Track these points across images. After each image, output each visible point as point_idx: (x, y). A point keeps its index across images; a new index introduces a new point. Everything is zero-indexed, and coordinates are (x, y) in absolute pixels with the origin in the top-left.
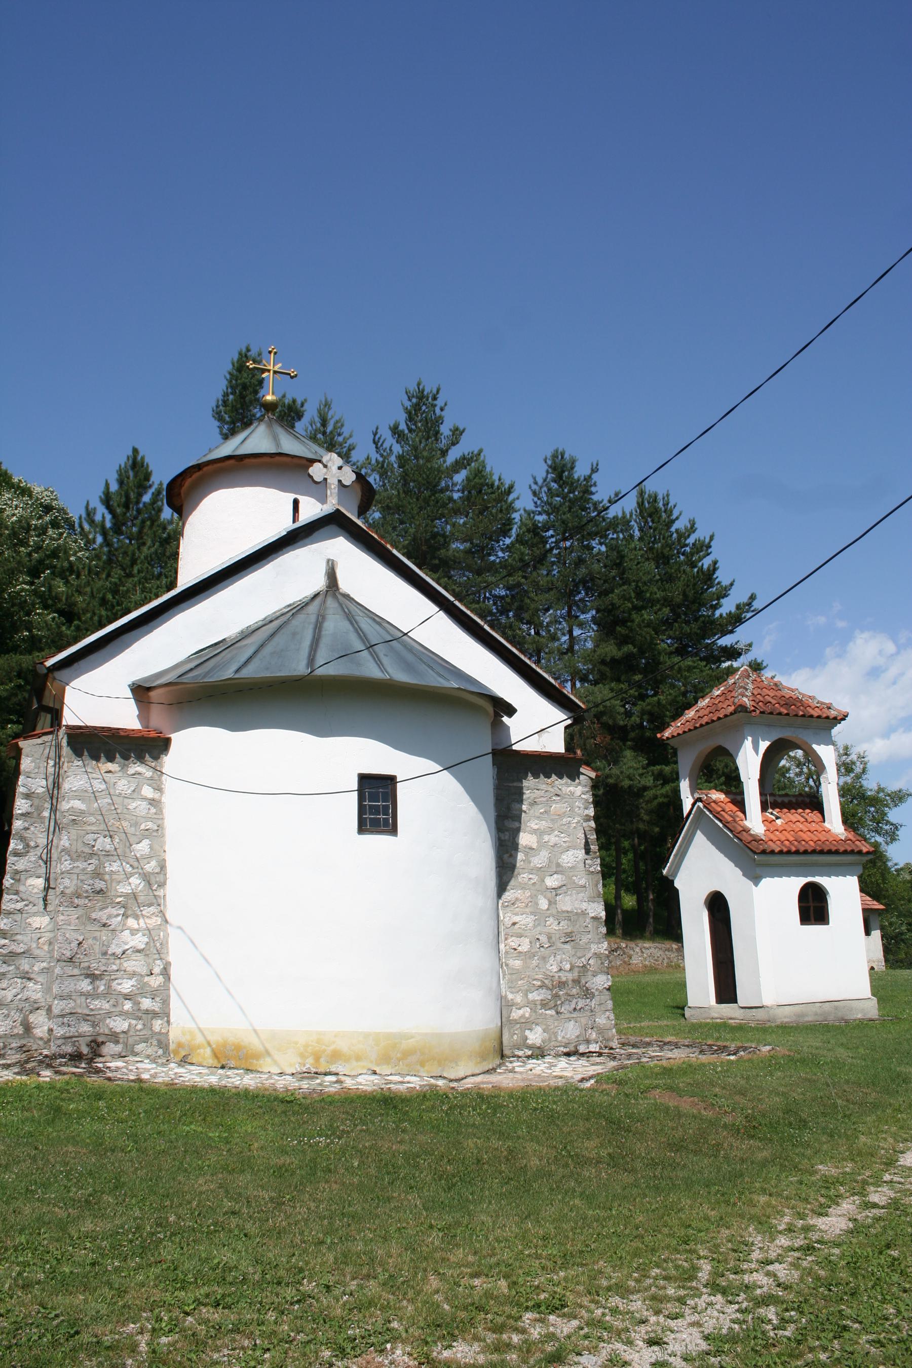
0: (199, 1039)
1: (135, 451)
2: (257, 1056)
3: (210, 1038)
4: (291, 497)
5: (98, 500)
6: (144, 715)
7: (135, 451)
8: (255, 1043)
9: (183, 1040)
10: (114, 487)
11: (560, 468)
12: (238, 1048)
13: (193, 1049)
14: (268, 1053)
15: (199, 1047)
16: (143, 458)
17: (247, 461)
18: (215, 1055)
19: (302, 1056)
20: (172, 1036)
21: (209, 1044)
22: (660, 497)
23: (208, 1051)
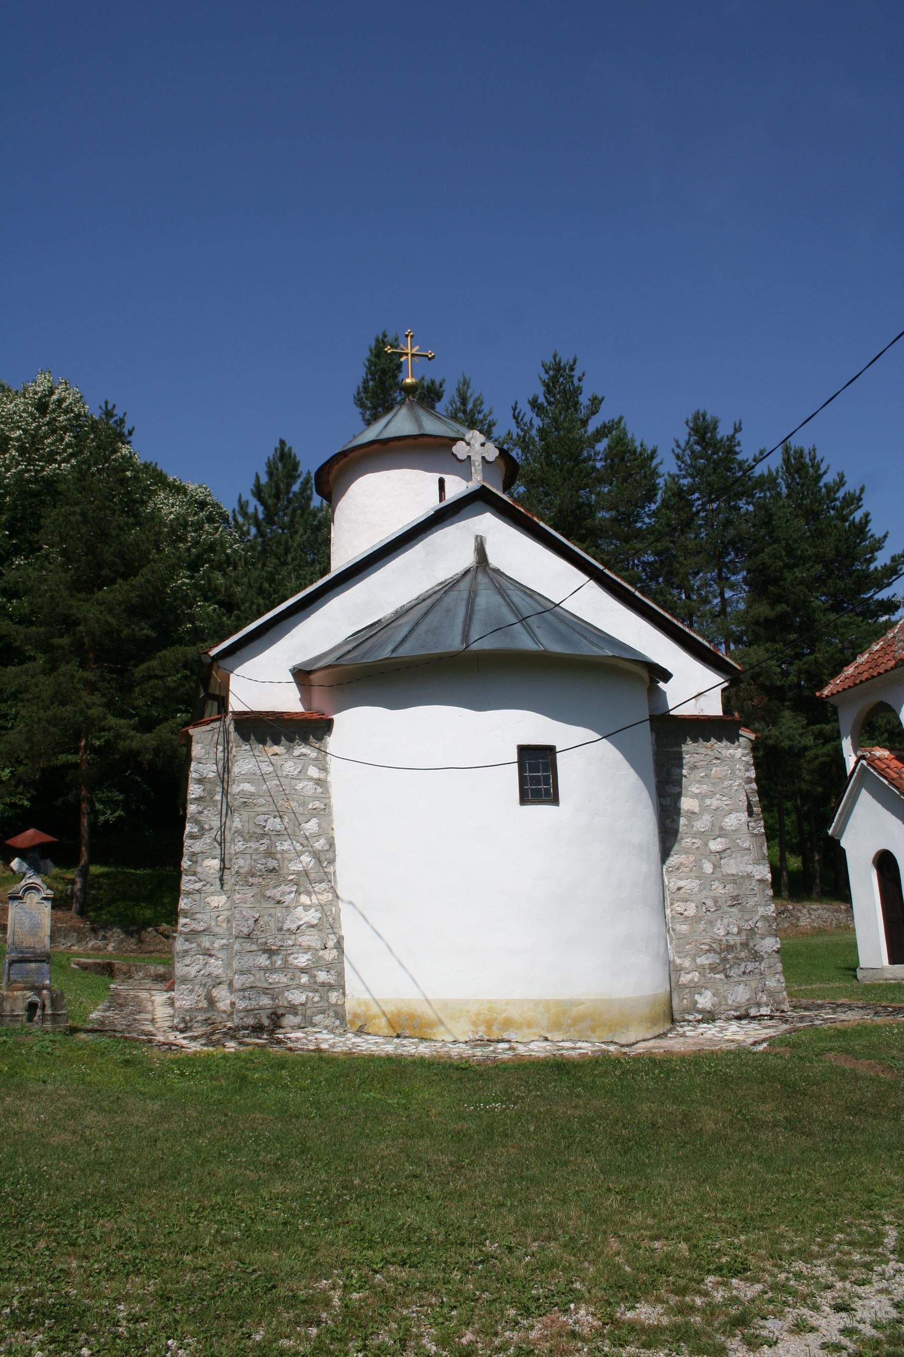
0: (375, 1010)
1: (282, 443)
2: (431, 1025)
3: (384, 1008)
5: (250, 492)
6: (306, 699)
8: (428, 1013)
10: (264, 479)
12: (412, 1017)
13: (369, 1019)
14: (441, 1022)
15: (374, 1017)
16: (290, 449)
17: (391, 444)
18: (391, 1024)
19: (474, 1024)
20: (348, 1007)
21: (384, 1014)
23: (383, 1021)
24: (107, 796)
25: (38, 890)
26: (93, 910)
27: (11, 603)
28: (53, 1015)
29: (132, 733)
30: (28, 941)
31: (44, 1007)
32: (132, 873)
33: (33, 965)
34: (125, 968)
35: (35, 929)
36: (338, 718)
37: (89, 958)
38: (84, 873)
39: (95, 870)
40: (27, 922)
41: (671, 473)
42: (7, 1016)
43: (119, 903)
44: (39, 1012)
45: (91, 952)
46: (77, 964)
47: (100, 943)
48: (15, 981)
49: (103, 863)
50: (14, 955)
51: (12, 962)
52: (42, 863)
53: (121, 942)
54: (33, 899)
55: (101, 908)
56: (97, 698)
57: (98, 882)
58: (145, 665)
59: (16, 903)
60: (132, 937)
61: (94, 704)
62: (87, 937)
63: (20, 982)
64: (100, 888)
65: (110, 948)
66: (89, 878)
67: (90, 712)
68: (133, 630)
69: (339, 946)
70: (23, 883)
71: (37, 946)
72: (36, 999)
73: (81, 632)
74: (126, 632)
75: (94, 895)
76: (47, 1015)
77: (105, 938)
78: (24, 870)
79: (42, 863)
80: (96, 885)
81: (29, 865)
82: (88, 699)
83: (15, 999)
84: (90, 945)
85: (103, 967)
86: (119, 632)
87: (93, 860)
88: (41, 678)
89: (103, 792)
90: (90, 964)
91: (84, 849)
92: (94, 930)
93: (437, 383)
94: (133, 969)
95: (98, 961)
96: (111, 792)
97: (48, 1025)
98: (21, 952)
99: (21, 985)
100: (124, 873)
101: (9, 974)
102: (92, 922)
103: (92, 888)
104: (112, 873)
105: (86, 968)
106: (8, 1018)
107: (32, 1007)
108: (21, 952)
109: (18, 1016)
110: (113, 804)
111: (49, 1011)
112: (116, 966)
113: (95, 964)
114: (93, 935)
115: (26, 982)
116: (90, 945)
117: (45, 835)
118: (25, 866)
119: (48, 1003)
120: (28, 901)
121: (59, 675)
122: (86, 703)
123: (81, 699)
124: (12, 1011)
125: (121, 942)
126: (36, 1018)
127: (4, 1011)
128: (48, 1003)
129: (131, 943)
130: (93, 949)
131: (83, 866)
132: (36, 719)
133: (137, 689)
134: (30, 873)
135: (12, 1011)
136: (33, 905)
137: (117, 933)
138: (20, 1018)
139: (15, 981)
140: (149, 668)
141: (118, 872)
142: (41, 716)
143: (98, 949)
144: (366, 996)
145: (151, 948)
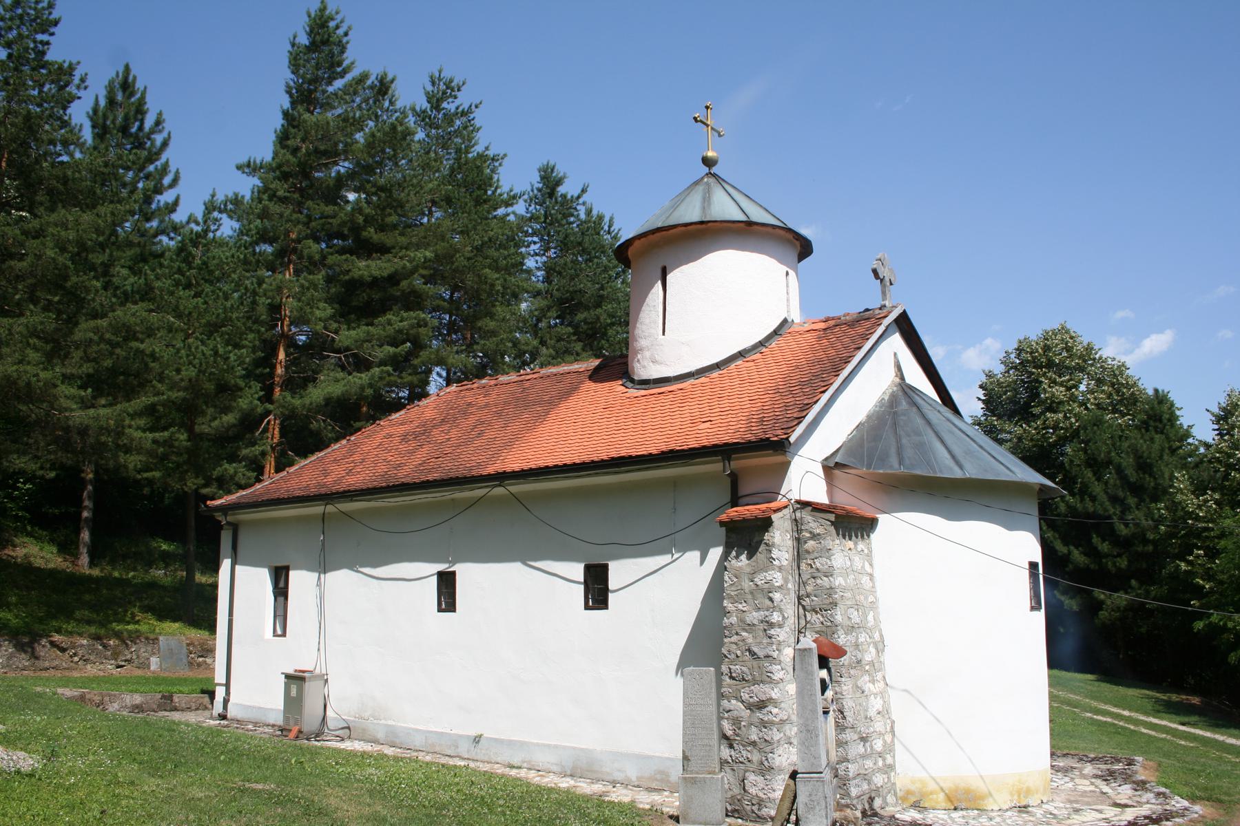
0: (932, 786)
1: (127, 69)
2: (982, 798)
3: (942, 784)
4: (785, 268)
5: (84, 115)
6: (830, 493)
7: (127, 69)
8: (977, 785)
9: (913, 788)
10: (102, 103)
11: (550, 181)
12: (968, 792)
13: (924, 795)
14: (990, 794)
15: (931, 793)
16: (135, 78)
17: (756, 227)
18: (949, 799)
19: (1012, 794)
20: (898, 786)
21: (942, 789)
22: (607, 219)
23: (941, 796)
36: (883, 519)
41: (77, 102)
69: (893, 731)
93: (390, 77)
94: (106, 699)
117: (1116, 688)
129: (23, 660)
144: (923, 775)
145: (47, 664)
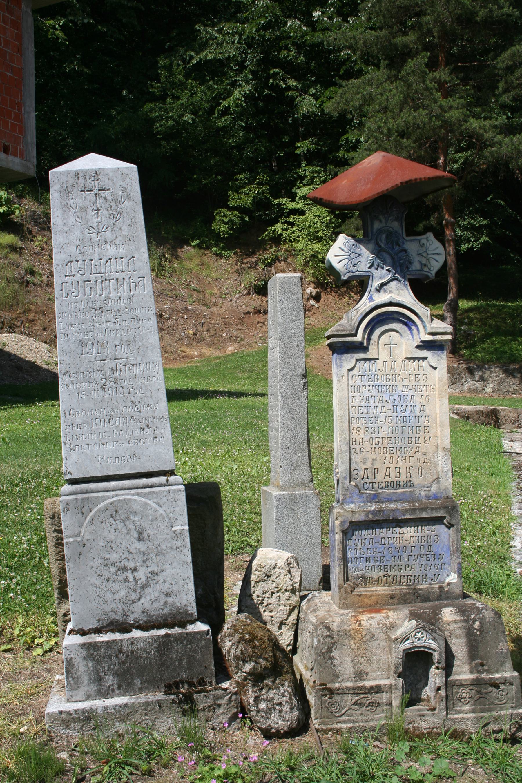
24: (469, 223)
25: (408, 323)
26: (466, 348)
27: (348, 22)
28: (477, 683)
29: (499, 137)
30: (391, 467)
31: (448, 668)
32: (504, 307)
33: (409, 533)
34: (513, 416)
35: (408, 431)
37: (469, 404)
38: (454, 308)
39: (464, 304)
40: (385, 416)
42: (343, 692)
43: (494, 339)
44: (435, 677)
45: (468, 395)
46: (457, 414)
47: (478, 385)
48: (365, 580)
49: (470, 297)
50: (357, 509)
51: (352, 528)
52: (412, 247)
53: (501, 382)
54: (396, 346)
55: (474, 345)
56: (455, 101)
57: (468, 318)
58: (509, 52)
59: (349, 360)
60: (514, 377)
61: (451, 107)
62: (462, 378)
63: (377, 582)
64: (470, 323)
65: (489, 389)
66: (459, 312)
67: (447, 115)
68: (491, 11)
70: (365, 304)
71: (416, 480)
72: (425, 641)
73: (427, 23)
74: (482, 13)
75: (465, 332)
76: (460, 684)
77: (482, 379)
78: (363, 267)
79: (412, 247)
80: (466, 321)
81: (378, 252)
82: (443, 102)
83: (366, 639)
84: (466, 386)
85: (487, 416)
86: (474, 13)
87: (462, 294)
88: (386, 86)
89: (464, 220)
90: (472, 413)
91: (451, 280)
92: (471, 371)
95: (481, 408)
96: (473, 218)
97: (465, 716)
98: (375, 498)
99: (382, 590)
100: (495, 305)
101: (344, 559)
102: (467, 361)
103: (462, 323)
104: (481, 306)
105: (468, 418)
106: (350, 699)
107: (415, 665)
108: (375, 498)
109: (378, 689)
110: (477, 230)
111: (463, 673)
112: (502, 414)
113: (478, 412)
114: (468, 375)
115: (394, 581)
116: (466, 386)
118: (366, 255)
119: (459, 647)
120: (383, 355)
121: (408, 74)
122: (441, 107)
123: (435, 102)
124: (360, 675)
125: (501, 382)
126: (428, 692)
127: (336, 676)
128: (459, 647)
130: (469, 391)
131: (451, 300)
132: (385, 130)
133: (501, 85)
134: (381, 275)
135: (360, 675)
136: (398, 366)
137: (496, 374)
138: (384, 697)
139: (365, 580)
140: (514, 54)
141: (488, 305)
142: (390, 126)
143: (476, 391)
